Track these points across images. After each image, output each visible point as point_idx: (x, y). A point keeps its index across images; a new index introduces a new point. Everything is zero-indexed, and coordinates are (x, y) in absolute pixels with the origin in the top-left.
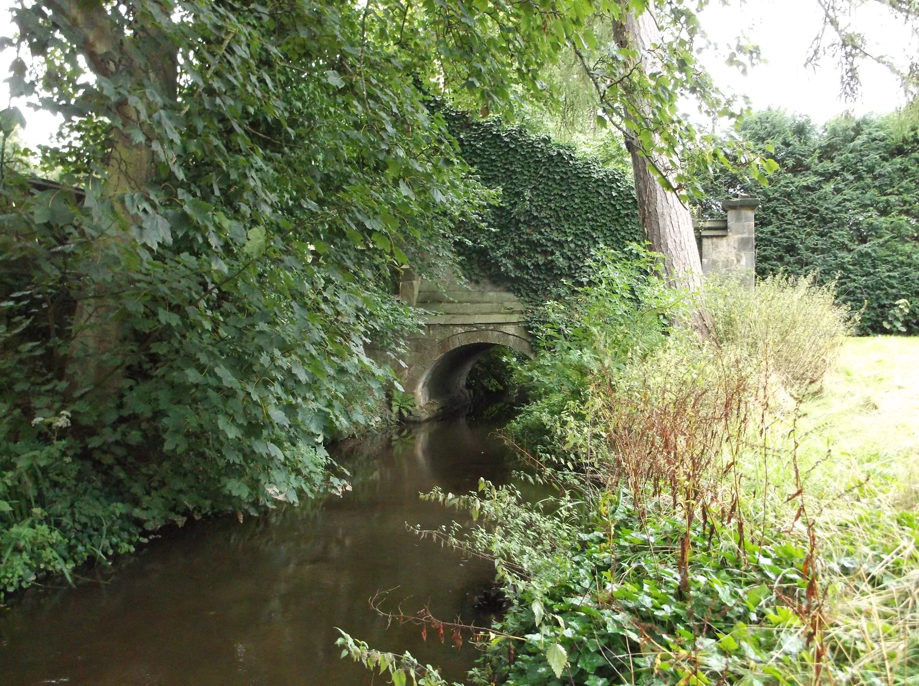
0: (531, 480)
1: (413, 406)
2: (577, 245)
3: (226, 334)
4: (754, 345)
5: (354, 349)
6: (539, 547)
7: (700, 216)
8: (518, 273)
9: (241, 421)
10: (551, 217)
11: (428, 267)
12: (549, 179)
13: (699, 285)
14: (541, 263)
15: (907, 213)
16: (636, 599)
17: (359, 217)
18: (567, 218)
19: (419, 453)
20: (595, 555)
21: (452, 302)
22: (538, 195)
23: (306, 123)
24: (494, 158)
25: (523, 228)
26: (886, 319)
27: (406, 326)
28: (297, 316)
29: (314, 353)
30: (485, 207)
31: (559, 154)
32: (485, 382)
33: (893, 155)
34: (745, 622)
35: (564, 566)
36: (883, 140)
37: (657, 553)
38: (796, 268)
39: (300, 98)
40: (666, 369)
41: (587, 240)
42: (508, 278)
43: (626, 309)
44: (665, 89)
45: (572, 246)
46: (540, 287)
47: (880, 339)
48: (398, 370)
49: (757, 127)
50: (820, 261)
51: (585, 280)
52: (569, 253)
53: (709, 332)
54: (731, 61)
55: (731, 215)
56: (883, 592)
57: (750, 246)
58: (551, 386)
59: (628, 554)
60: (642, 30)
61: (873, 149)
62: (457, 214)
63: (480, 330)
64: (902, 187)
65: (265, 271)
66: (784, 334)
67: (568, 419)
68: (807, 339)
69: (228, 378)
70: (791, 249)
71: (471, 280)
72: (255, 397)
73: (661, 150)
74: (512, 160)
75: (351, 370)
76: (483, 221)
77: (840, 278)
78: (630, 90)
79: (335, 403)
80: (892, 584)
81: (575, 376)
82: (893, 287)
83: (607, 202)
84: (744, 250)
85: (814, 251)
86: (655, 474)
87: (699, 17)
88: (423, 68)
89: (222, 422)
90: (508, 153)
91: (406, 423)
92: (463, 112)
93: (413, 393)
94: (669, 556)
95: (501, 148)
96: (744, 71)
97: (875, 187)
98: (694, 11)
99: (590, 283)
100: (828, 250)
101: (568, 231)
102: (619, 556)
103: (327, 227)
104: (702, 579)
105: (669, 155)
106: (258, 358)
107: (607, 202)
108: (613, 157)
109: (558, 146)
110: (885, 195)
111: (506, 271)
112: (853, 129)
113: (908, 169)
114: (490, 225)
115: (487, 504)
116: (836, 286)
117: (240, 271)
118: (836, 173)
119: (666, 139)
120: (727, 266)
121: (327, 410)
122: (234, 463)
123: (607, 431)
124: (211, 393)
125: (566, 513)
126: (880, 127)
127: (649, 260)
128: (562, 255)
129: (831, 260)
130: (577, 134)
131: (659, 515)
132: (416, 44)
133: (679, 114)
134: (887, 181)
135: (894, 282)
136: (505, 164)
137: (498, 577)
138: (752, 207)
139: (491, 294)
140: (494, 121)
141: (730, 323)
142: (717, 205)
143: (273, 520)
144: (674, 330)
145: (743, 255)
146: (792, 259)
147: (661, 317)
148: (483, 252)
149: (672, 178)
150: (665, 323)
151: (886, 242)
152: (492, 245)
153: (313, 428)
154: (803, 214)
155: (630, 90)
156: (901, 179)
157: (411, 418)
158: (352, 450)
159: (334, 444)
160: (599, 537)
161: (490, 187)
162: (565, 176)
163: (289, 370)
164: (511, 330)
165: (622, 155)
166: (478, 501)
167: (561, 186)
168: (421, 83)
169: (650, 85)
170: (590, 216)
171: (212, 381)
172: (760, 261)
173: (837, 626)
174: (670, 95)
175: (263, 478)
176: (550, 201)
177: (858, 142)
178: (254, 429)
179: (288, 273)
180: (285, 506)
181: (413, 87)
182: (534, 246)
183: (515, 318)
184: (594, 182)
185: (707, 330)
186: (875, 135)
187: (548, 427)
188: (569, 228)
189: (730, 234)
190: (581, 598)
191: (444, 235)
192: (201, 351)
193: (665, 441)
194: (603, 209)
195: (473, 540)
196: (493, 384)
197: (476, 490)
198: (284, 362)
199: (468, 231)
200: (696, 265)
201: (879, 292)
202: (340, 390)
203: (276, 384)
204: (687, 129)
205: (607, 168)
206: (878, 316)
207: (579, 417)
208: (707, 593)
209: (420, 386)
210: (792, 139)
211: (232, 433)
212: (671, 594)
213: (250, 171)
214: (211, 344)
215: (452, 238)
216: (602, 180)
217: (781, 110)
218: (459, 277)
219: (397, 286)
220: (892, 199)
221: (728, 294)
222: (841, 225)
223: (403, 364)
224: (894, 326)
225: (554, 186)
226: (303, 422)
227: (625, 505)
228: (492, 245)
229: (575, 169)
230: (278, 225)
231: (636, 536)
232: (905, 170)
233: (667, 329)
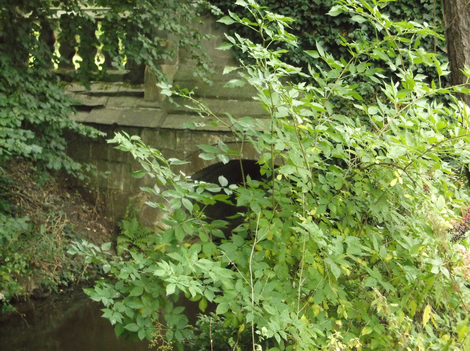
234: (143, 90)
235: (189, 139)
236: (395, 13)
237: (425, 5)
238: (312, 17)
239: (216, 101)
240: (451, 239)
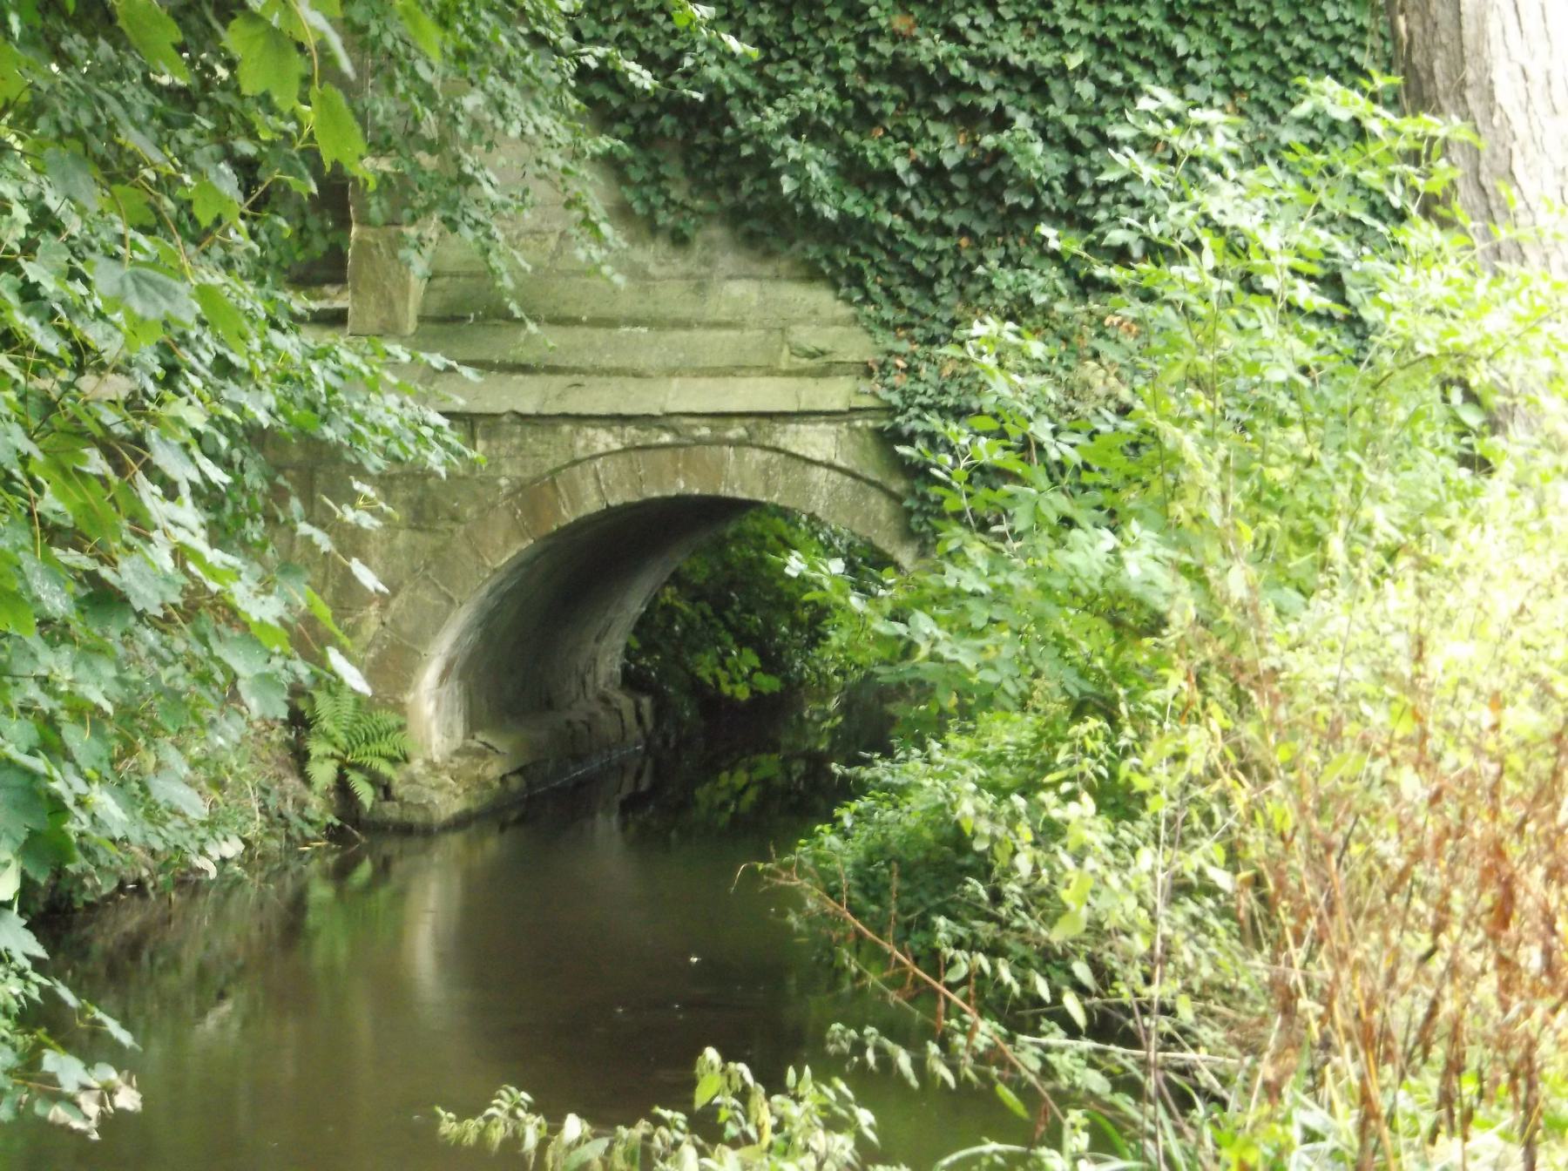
2: (1103, 87)
8: (854, 205)
14: (949, 161)
32: (705, 667)
42: (811, 220)
46: (946, 266)
52: (1072, 121)
58: (990, 677)
81: (1092, 643)
91: (366, 834)
93: (399, 708)
99: (1156, 251)
101: (1068, 25)
111: (801, 196)
128: (1041, 128)
139: (737, 289)
144: (1506, 449)
147: (1456, 395)
157: (392, 811)
158: (134, 946)
164: (818, 441)
182: (923, 86)
183: (836, 393)
196: (739, 676)
209: (429, 676)
228: (747, 81)
234: (339, 304)
235: (516, 441)
236: (1108, 83)
237: (1190, 63)
238: (871, 89)
239: (579, 332)
240: (1070, 829)
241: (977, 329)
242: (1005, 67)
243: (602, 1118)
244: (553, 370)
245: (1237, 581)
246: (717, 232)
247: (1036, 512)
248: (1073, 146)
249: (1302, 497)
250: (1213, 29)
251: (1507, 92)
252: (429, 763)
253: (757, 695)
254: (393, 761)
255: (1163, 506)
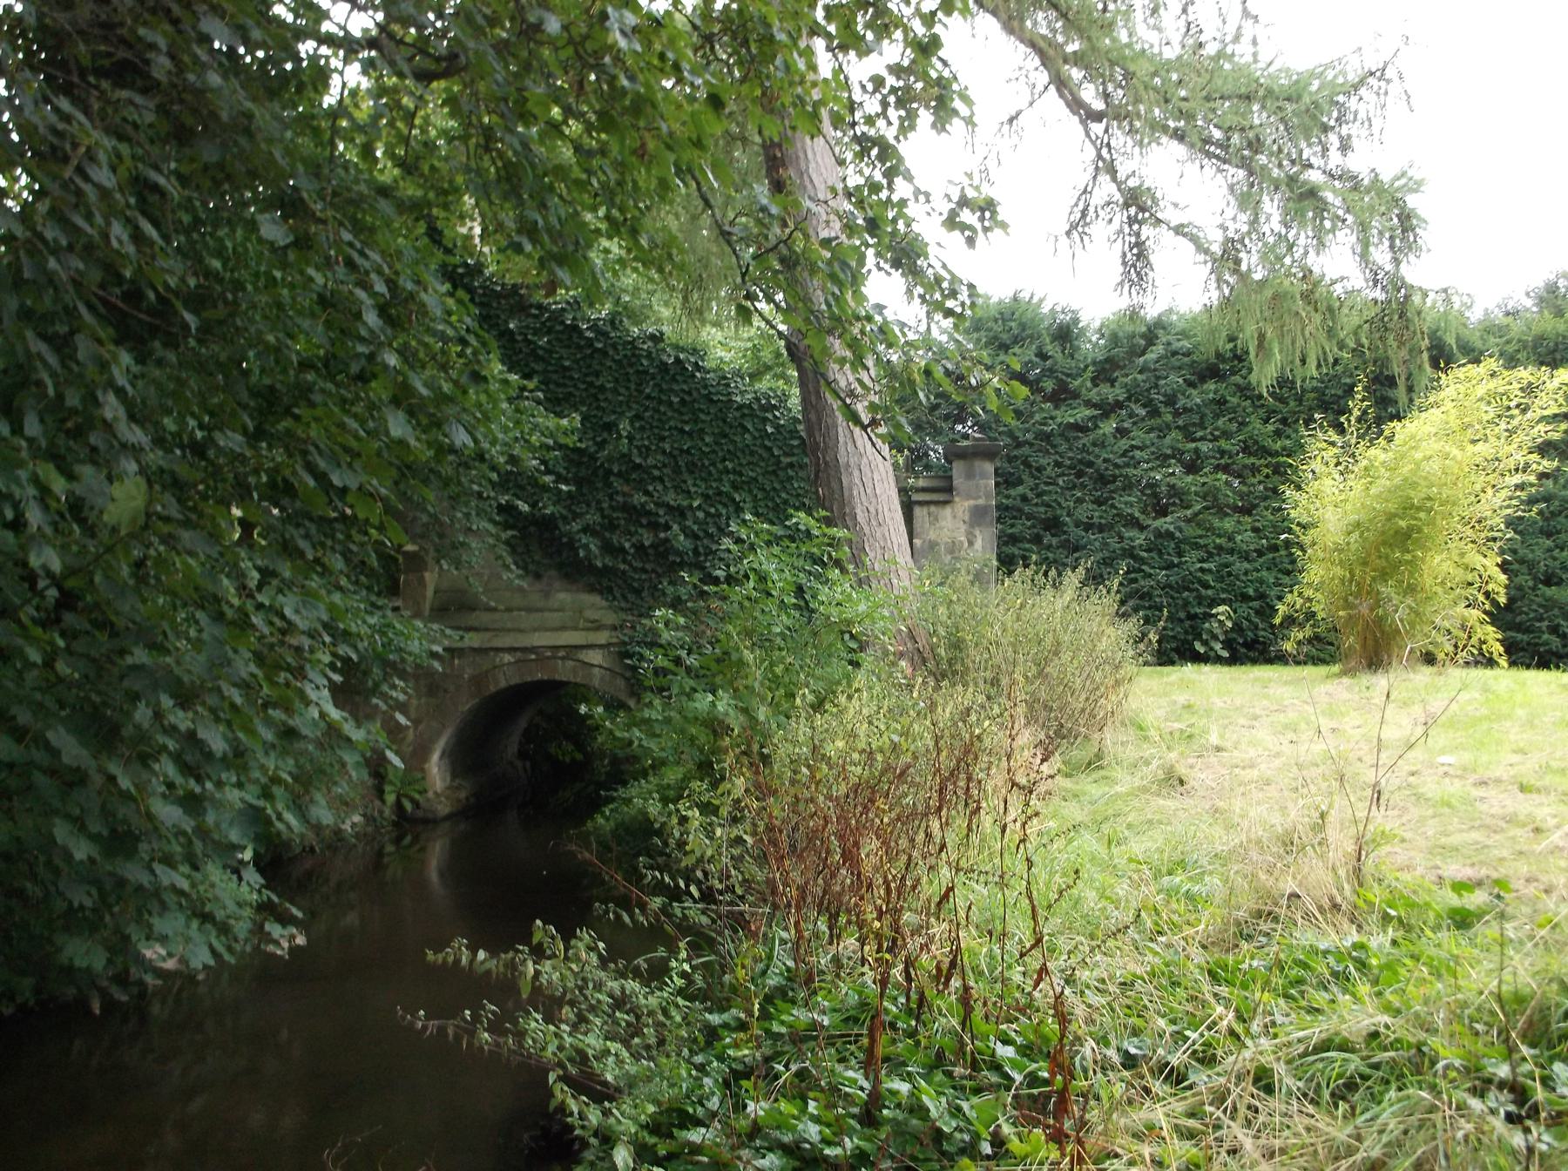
0: (626, 918)
1: (423, 792)
2: (708, 514)
3: (69, 671)
4: (995, 682)
5: (312, 695)
6: (637, 1040)
7: (910, 467)
8: (609, 561)
9: (95, 827)
10: (665, 466)
11: (450, 550)
12: (660, 402)
13: (907, 583)
14: (647, 543)
15: (1225, 469)
16: (793, 1129)
17: (322, 464)
18: (692, 468)
19: (434, 876)
20: (730, 1052)
21: (495, 610)
22: (642, 428)
23: (230, 296)
24: (567, 363)
25: (617, 484)
26: (1198, 636)
27: (410, 654)
28: (205, 636)
29: (238, 700)
30: (549, 448)
31: (678, 361)
32: (553, 750)
33: (1203, 379)
34: (973, 1159)
35: (676, 1076)
36: (1187, 354)
37: (833, 1044)
38: (1061, 554)
39: (220, 253)
40: (861, 723)
41: (725, 505)
42: (591, 568)
43: (789, 622)
44: (845, 265)
45: (701, 515)
46: (647, 585)
47: (1189, 670)
48: (394, 731)
49: (998, 328)
50: (1097, 544)
51: (720, 573)
52: (695, 528)
53: (924, 661)
54: (952, 222)
55: (958, 469)
56: (1189, 1093)
57: (988, 519)
58: (664, 754)
59: (786, 1048)
60: (812, 165)
61: (1173, 368)
62: (502, 460)
63: (541, 660)
64: (1216, 429)
65: (146, 557)
66: (1041, 665)
67: (690, 813)
68: (1077, 673)
69: (70, 748)
70: (1053, 525)
71: (525, 568)
72: (125, 783)
73: (842, 361)
74: (598, 368)
75: (305, 731)
76: (548, 472)
77: (1127, 573)
78: (790, 263)
79: (278, 791)
80: (1200, 1078)
81: (703, 737)
82: (1206, 586)
83: (758, 442)
84: (979, 525)
85: (1088, 527)
86: (831, 908)
87: (903, 148)
88: (446, 206)
89: (61, 831)
90: (591, 356)
91: (410, 823)
92: (514, 286)
93: (423, 770)
94: (853, 1047)
95: (579, 348)
96: (971, 242)
97: (1178, 427)
98: (892, 141)
99: (730, 580)
100: (1110, 527)
101: (693, 489)
102: (768, 1052)
103: (264, 479)
104: (904, 1088)
105: (854, 369)
106: (129, 715)
107: (758, 442)
108: (768, 368)
109: (677, 347)
110: (1194, 440)
111: (587, 557)
112: (1143, 336)
113: (1226, 401)
114: (560, 479)
115: (547, 966)
116: (1121, 584)
117: (98, 558)
118: (1119, 405)
119: (850, 346)
120: (951, 552)
121: (261, 803)
122: (82, 907)
123: (754, 834)
124: (40, 779)
125: (679, 982)
126: (1184, 334)
127: (826, 540)
128: (684, 530)
129: (1113, 542)
130: (708, 328)
131: (838, 976)
132: (433, 168)
133: (868, 306)
134: (1196, 419)
135: (1209, 578)
136: (586, 375)
137: (553, 1104)
138: (989, 455)
139: (562, 596)
140: (568, 303)
141: (957, 645)
142: (937, 452)
143: (156, 1009)
144: (867, 659)
145: (977, 533)
146: (1055, 541)
147: (847, 637)
148: (548, 524)
149: (860, 408)
150: (855, 646)
151: (1196, 515)
152: (564, 512)
153: (234, 836)
154: (1070, 468)
155: (790, 263)
156: (1217, 416)
157: (420, 814)
158: (309, 874)
159: (276, 862)
160: (739, 1019)
161: (560, 415)
162: (687, 398)
163: (191, 735)
164: (595, 657)
165: (783, 365)
166: (530, 964)
167: (682, 414)
168: (440, 233)
169: (820, 257)
170: (729, 465)
171: (39, 756)
172: (1006, 544)
173: (1117, 1156)
174: (853, 276)
175: (134, 932)
176: (663, 439)
177: (1151, 356)
178: (120, 842)
179: (190, 561)
180: (178, 983)
181: (426, 240)
182: (636, 514)
183: (602, 637)
184: (737, 409)
185: (920, 659)
186: (1176, 345)
187: (657, 826)
188: (695, 485)
189: (957, 499)
190: (703, 1130)
191: (480, 495)
192: (20, 702)
193: (838, 853)
194: (752, 453)
195: (521, 1035)
196: (565, 751)
197: (528, 943)
198: (181, 720)
199: (522, 488)
200: (903, 553)
201: (1186, 594)
202: (285, 769)
203: (164, 758)
204: (881, 329)
205: (757, 386)
206: (1186, 632)
207: (708, 809)
208: (911, 1111)
209: (436, 757)
210: (1051, 349)
211: (82, 851)
212: (853, 1116)
213: (105, 391)
214: (39, 689)
215: (495, 499)
216: (749, 406)
217: (1035, 300)
218: (507, 567)
219: (396, 582)
220: (1205, 447)
221: (954, 598)
222: (1128, 487)
223: (402, 719)
224: (1212, 649)
225: (670, 414)
226: (217, 825)
227: (784, 960)
228: (564, 512)
229: (706, 387)
230: (172, 473)
231: (801, 1016)
232: (1222, 402)
233: (855, 657)
241: (657, 613)
242: (668, 505)
243: (493, 952)
244: (487, 630)
245: (762, 713)
246: (553, 573)
247: (681, 686)
248: (696, 537)
249: (787, 679)
250: (750, 491)
251: (861, 517)
252: (435, 793)
253: (573, 760)
254: (420, 793)
255: (731, 683)
